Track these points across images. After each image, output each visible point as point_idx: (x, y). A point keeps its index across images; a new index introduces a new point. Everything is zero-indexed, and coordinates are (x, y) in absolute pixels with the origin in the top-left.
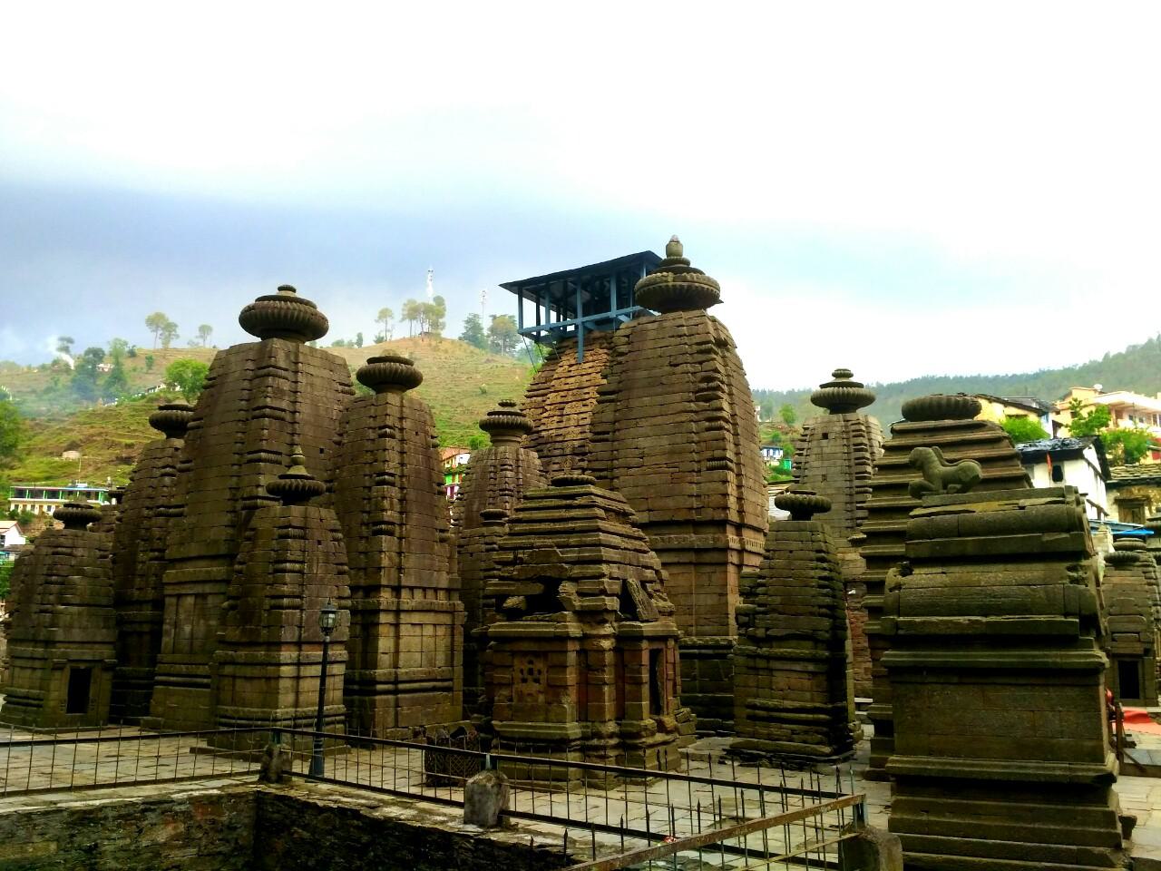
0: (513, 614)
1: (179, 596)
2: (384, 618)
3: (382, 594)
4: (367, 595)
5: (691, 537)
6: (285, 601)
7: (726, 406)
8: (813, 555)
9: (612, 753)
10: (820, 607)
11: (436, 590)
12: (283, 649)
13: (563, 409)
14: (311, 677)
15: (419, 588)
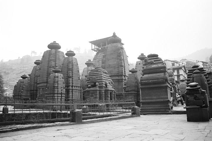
0: (89, 87)
1: (40, 89)
7: (122, 57)
11: (78, 87)
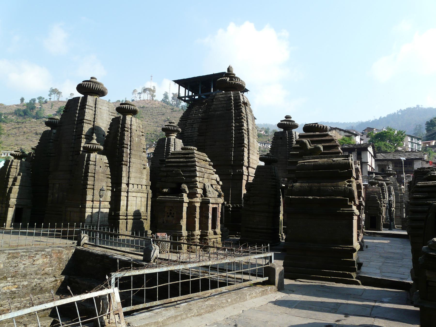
13: (193, 126)
15: (136, 184)
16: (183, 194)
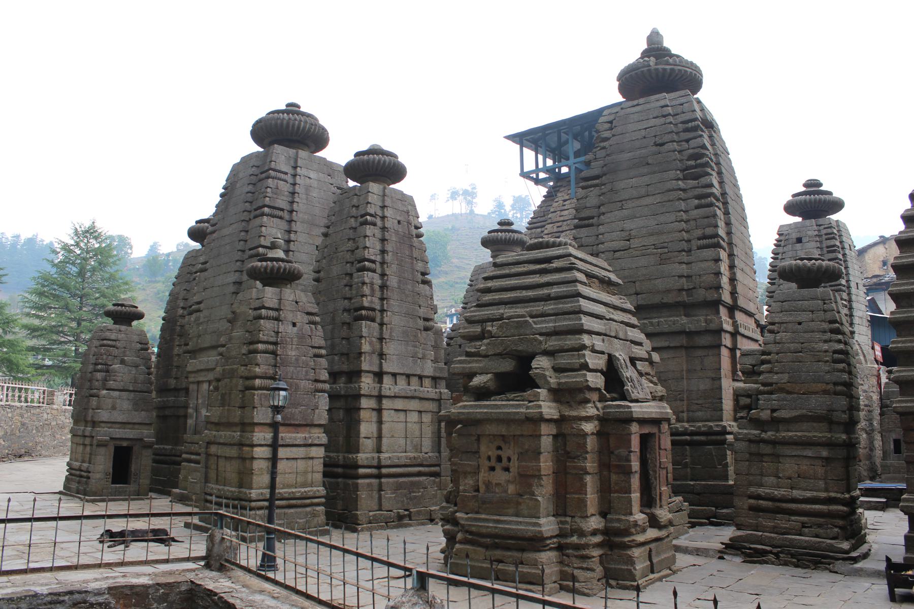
0: (482, 394)
1: (199, 383)
2: (365, 403)
3: (363, 379)
4: (350, 381)
5: (681, 319)
6: (258, 382)
8: (826, 326)
9: (596, 553)
10: (835, 384)
11: (421, 377)
12: (256, 430)
14: (287, 459)
15: (402, 374)
16: (539, 390)
